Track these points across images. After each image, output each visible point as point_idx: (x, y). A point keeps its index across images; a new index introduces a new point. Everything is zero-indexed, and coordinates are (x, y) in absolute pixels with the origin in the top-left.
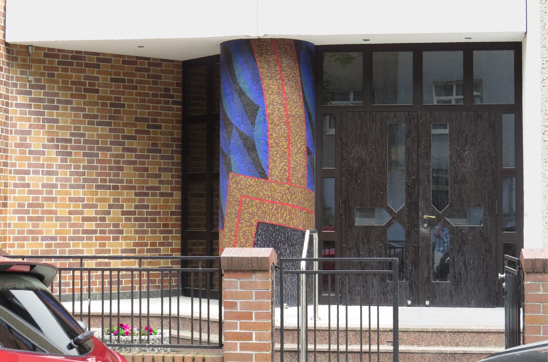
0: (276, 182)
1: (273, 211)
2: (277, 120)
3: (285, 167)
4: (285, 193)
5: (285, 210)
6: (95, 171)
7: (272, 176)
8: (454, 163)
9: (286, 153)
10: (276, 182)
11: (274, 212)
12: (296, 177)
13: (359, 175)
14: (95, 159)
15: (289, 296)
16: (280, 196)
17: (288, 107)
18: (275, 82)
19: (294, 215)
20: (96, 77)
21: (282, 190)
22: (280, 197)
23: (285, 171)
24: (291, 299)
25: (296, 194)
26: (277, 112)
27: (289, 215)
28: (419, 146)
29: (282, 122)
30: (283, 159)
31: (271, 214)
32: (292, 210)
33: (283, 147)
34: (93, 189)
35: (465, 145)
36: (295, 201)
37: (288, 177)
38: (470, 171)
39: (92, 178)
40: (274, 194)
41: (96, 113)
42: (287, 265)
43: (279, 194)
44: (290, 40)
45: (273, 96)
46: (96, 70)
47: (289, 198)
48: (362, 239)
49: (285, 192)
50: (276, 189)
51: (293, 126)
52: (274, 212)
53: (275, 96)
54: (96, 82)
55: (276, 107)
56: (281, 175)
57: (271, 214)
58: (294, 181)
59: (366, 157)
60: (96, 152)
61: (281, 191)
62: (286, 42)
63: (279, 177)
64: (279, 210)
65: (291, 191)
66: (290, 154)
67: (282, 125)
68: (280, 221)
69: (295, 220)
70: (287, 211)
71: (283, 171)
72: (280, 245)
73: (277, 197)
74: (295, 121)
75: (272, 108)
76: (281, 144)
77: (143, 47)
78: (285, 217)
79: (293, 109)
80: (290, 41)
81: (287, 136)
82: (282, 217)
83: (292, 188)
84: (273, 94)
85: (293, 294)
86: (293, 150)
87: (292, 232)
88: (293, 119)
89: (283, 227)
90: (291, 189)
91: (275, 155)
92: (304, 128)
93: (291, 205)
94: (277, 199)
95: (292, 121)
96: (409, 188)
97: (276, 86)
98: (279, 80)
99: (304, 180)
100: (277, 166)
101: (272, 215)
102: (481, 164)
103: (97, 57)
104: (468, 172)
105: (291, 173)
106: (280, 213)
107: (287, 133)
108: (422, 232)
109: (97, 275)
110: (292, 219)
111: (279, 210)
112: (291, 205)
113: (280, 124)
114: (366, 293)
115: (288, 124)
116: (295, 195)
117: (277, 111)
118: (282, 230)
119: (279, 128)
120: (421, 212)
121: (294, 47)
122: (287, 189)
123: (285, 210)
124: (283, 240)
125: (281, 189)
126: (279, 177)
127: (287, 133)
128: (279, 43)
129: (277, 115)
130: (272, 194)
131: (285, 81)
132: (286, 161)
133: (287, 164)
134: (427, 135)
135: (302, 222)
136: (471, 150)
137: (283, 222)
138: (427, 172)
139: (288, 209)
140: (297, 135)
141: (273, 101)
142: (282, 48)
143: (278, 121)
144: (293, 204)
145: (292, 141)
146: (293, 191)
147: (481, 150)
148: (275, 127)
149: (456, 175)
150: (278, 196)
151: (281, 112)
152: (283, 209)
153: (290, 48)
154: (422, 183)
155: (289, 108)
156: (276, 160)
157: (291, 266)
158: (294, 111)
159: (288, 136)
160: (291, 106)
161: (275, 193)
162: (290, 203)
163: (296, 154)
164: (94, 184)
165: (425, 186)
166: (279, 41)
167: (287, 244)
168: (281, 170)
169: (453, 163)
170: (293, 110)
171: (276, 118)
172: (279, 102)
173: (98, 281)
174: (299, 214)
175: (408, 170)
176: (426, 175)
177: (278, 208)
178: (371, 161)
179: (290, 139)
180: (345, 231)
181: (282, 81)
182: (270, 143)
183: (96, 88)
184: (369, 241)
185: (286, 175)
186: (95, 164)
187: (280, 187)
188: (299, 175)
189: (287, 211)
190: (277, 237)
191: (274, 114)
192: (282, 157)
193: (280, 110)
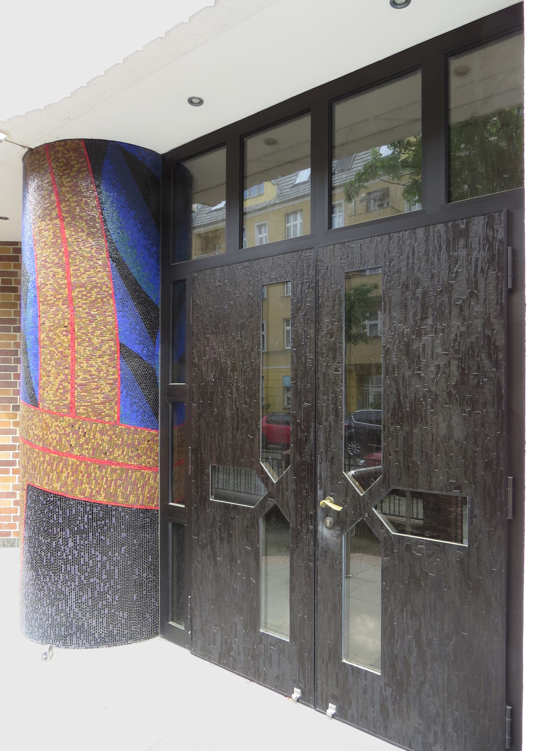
0: (50, 412)
1: (45, 467)
2: (51, 296)
3: (64, 384)
4: (64, 434)
5: (65, 465)
6: (12, 389)
7: (43, 400)
8: (394, 369)
9: (68, 357)
10: (50, 412)
11: (47, 468)
12: (88, 402)
13: (215, 397)
14: (12, 373)
15: (74, 629)
16: (56, 438)
17: (71, 269)
18: (49, 225)
19: (83, 476)
20: (13, 272)
21: (60, 428)
22: (55, 441)
23: (66, 392)
24: (78, 634)
25: (89, 435)
26: (52, 281)
27: (73, 476)
28: (317, 331)
29: (60, 298)
30: (61, 368)
31: (42, 472)
32: (80, 465)
33: (62, 345)
34: (10, 411)
35: (422, 319)
36: (87, 449)
37: (71, 403)
38: (433, 389)
39: (8, 397)
40: (46, 435)
41: (12, 317)
42: (69, 568)
43: (54, 435)
44: (76, 141)
45: (47, 252)
46: (13, 263)
47: (73, 443)
48: (220, 530)
49: (65, 431)
50: (50, 425)
51: (82, 304)
52: (47, 468)
53: (49, 250)
54: (13, 278)
55: (50, 272)
56: (57, 398)
57: (42, 472)
58: (84, 409)
59: (226, 360)
60: (13, 365)
61: (57, 428)
62: (68, 146)
63: (54, 402)
64: (55, 465)
65: (77, 428)
66: (74, 360)
67: (60, 304)
68: (55, 485)
69: (86, 485)
70: (69, 468)
71: (62, 391)
72: (55, 531)
73: (51, 441)
74: (85, 295)
75: (44, 273)
76: (57, 340)
77: (6, 219)
78: (65, 478)
79: (83, 271)
80: (76, 144)
81: (68, 324)
82: (59, 478)
83: (80, 423)
84: (46, 247)
85: (83, 625)
86: (82, 351)
87: (80, 507)
88: (82, 291)
89: (62, 498)
90: (77, 426)
91: (49, 362)
92: (110, 307)
93: (76, 457)
94: (51, 443)
95: (80, 296)
96: (299, 429)
97: (51, 231)
98: (55, 218)
99: (112, 408)
100: (51, 382)
101: (44, 475)
102: (463, 369)
103: (13, 248)
104: (430, 391)
105: (76, 394)
106: (56, 470)
107: (68, 319)
108: (322, 536)
109: (17, 516)
110: (79, 482)
111: (55, 465)
112: (76, 457)
113: (56, 303)
114: (226, 643)
115: (71, 301)
116: (87, 436)
117: (52, 278)
118: (59, 503)
119: (54, 309)
120: (321, 488)
121: (86, 153)
122: (68, 426)
123: (65, 465)
124: (61, 521)
125: (58, 426)
126: (54, 402)
127: (68, 319)
128: (56, 149)
129: (51, 286)
130: (43, 434)
131: (66, 220)
132: (67, 371)
133: (69, 377)
134: (334, 300)
135: (104, 489)
136: (436, 332)
137: (61, 487)
138: (334, 392)
139: (70, 463)
140: (91, 322)
141: (45, 261)
142: (61, 158)
143: (53, 297)
144: (81, 455)
145: (79, 334)
146: (81, 430)
147: (463, 329)
148: (49, 309)
149: (399, 400)
150: (52, 438)
151: (59, 280)
152: (61, 464)
153: (76, 157)
154: (324, 417)
155: (73, 270)
156: (50, 371)
157: (77, 571)
158: (85, 276)
159: (72, 324)
160: (77, 267)
161: (49, 433)
162: (76, 452)
163: (88, 360)
164: (11, 405)
165: (330, 426)
166: (57, 146)
167: (68, 530)
168: (57, 390)
169: (391, 369)
170: (82, 274)
171: (51, 292)
172: (56, 262)
173: (17, 523)
174: (96, 473)
175: (297, 387)
176: (331, 398)
177: (52, 461)
178: (234, 369)
179: (74, 330)
180: (196, 508)
181: (60, 220)
182: (41, 339)
183: (13, 285)
184: (230, 535)
185: (67, 398)
186: (12, 380)
187: (57, 421)
188: (98, 398)
189: (69, 468)
190: (50, 515)
191: (47, 285)
192: (60, 364)
193: (57, 276)
